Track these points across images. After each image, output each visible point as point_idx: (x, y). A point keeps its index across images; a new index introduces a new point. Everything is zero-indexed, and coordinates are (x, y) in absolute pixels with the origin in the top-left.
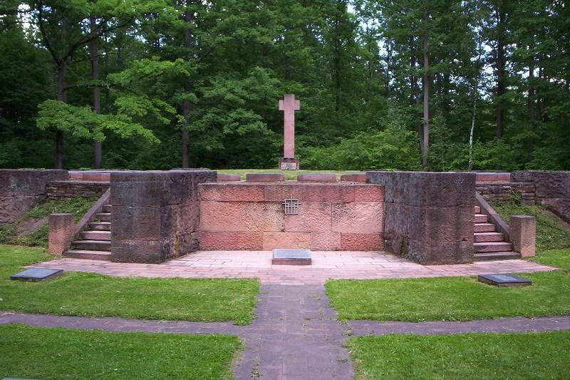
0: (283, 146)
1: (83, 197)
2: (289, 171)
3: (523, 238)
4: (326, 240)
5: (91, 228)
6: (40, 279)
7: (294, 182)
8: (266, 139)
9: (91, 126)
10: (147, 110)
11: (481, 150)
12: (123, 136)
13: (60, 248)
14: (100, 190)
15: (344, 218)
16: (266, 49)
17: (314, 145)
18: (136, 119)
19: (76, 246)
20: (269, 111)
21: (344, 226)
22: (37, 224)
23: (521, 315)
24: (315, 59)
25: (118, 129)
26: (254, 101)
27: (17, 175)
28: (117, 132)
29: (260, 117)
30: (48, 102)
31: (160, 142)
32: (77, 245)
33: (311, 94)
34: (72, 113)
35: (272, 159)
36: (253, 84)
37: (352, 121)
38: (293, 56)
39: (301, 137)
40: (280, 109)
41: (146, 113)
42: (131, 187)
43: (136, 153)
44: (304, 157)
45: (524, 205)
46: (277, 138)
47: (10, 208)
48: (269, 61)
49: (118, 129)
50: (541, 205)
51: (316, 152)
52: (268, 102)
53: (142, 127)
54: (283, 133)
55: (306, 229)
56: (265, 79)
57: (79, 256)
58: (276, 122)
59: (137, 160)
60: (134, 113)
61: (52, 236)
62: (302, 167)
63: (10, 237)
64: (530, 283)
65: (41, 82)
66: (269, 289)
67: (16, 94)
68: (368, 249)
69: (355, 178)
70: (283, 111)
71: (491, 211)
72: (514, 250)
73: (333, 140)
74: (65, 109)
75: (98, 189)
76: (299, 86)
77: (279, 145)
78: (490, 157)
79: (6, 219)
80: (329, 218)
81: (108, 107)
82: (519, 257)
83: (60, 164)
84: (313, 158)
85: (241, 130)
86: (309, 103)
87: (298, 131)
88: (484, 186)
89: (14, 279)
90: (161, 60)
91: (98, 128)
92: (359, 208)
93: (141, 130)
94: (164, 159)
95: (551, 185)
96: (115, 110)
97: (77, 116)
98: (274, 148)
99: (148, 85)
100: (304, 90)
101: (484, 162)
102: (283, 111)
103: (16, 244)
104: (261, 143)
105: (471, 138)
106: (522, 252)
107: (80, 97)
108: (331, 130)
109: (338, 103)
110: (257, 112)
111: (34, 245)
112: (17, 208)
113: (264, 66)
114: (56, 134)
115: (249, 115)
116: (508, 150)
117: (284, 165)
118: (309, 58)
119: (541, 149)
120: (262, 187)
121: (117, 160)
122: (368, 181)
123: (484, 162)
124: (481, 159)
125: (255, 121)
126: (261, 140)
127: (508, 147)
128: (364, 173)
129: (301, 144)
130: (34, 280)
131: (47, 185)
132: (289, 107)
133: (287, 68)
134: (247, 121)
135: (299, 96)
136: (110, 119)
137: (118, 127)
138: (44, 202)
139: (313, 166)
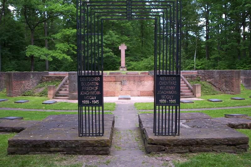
0: (121, 62)
1: (56, 81)
2: (123, 71)
3: (196, 91)
4: (135, 92)
5: (61, 90)
6: (51, 104)
7: (125, 75)
8: (113, 59)
9: (46, 55)
10: (68, 48)
11: (200, 63)
12: (59, 59)
13: (52, 96)
14: (61, 78)
15: (141, 86)
16: (113, 24)
17: (132, 61)
18: (64, 52)
19: (56, 96)
20: (115, 48)
21: (141, 89)
22: (41, 89)
23: (186, 108)
24: (133, 26)
25: (57, 56)
26: (109, 44)
27: (32, 74)
28: (57, 57)
29: (111, 50)
30: (30, 46)
31: (73, 61)
32: (57, 95)
33: (131, 40)
34: (39, 50)
35: (116, 67)
36: (108, 38)
37: (149, 51)
38: (124, 26)
39: (127, 58)
40: (120, 49)
41: (68, 50)
42: (75, 77)
43: (62, 65)
44: (128, 66)
45: (201, 81)
46: (118, 58)
47: (30, 84)
48: (114, 28)
49: (57, 56)
50: (207, 81)
51: (134, 64)
52: (114, 44)
53: (66, 55)
54: (120, 56)
55: (129, 90)
56: (112, 35)
57: (58, 99)
58: (118, 53)
59: (63, 68)
60: (63, 50)
61: (49, 92)
62: (128, 70)
63: (32, 94)
64: (193, 102)
65: (23, 37)
66: (118, 105)
67: (13, 42)
68: (148, 96)
69: (145, 73)
70: (120, 50)
71: (188, 83)
72: (194, 95)
73: (140, 59)
74: (36, 48)
75: (61, 78)
76: (126, 38)
77: (119, 61)
78: (202, 65)
79: (29, 88)
80: (136, 86)
81: (51, 47)
82: (196, 97)
83: (33, 70)
84: (132, 66)
85: (104, 55)
86: (131, 44)
87: (126, 55)
88: (187, 75)
89: (43, 104)
90: (73, 29)
91: (49, 56)
92: (146, 83)
93: (66, 56)
94: (73, 67)
95: (210, 75)
96: (55, 49)
97: (41, 51)
98: (117, 63)
99: (66, 39)
100: (128, 39)
101: (199, 67)
102: (120, 50)
103: (35, 96)
104: (111, 61)
105: (195, 57)
106: (196, 95)
107: (41, 44)
108: (140, 54)
109: (142, 44)
110: (110, 48)
111: (41, 96)
112: (33, 84)
113: (113, 30)
114: (32, 57)
115: (107, 49)
116: (209, 62)
117: (121, 69)
118: (130, 26)
119: (221, 61)
120: (115, 76)
121: (54, 68)
122: (149, 74)
123: (199, 67)
124: (198, 66)
125: (109, 52)
126: (111, 60)
127: (209, 61)
128: (147, 71)
129: (127, 61)
130: (49, 104)
131: (42, 77)
132: (123, 48)
133: (122, 31)
134: (106, 52)
135: (126, 42)
136: (54, 52)
137: (57, 55)
138: (41, 83)
139: (132, 69)
